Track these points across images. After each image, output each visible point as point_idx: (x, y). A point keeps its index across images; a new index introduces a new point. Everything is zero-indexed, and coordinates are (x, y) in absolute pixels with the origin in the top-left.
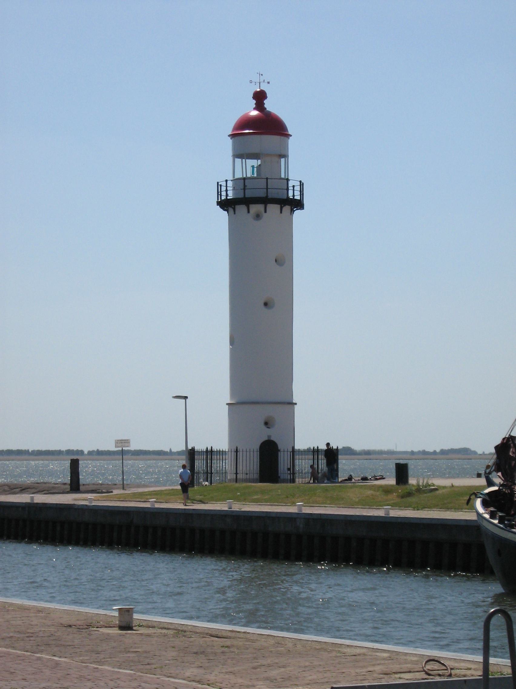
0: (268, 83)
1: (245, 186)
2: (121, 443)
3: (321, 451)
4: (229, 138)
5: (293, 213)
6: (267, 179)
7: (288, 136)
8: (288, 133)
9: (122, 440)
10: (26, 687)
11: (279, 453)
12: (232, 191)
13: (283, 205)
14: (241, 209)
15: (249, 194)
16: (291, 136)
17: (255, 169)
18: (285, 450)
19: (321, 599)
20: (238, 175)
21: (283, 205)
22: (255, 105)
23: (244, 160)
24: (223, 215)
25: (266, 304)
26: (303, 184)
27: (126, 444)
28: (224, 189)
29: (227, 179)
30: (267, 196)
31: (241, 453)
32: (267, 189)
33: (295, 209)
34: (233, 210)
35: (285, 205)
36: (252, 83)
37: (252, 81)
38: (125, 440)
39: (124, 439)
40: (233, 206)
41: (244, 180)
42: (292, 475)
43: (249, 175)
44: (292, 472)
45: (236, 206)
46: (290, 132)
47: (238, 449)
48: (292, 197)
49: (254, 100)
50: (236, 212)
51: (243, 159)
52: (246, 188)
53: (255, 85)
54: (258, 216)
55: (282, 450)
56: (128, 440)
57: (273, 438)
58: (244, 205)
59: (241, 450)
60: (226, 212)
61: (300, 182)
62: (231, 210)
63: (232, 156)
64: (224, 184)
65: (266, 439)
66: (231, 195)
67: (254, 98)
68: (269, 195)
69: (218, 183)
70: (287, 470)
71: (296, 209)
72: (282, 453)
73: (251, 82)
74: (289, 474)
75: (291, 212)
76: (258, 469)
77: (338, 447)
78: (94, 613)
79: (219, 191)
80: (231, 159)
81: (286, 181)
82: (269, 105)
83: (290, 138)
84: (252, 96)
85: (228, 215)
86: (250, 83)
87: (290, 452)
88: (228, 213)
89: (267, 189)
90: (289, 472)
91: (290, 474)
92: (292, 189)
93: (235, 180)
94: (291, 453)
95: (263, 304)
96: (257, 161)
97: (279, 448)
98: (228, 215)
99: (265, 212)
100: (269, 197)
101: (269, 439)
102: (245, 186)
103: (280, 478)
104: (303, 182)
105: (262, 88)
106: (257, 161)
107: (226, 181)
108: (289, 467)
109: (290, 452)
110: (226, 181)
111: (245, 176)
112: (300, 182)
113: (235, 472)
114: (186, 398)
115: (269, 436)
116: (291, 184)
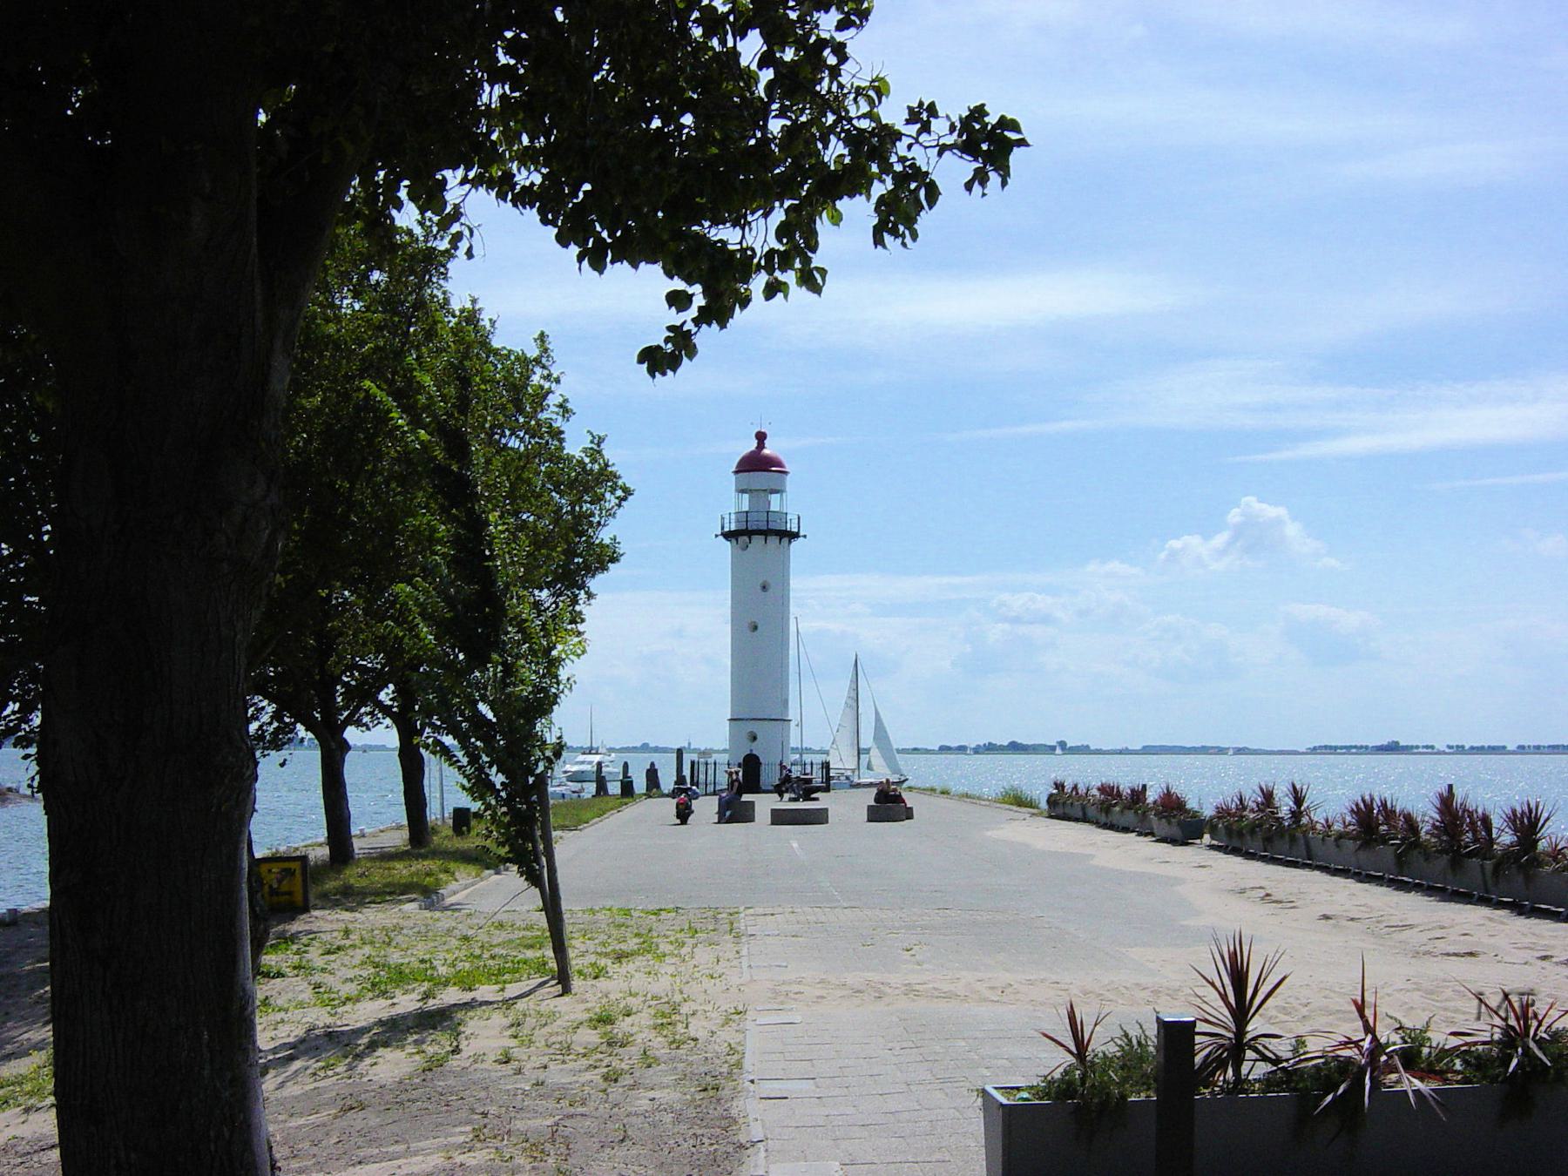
57: (754, 752)
62: (734, 541)
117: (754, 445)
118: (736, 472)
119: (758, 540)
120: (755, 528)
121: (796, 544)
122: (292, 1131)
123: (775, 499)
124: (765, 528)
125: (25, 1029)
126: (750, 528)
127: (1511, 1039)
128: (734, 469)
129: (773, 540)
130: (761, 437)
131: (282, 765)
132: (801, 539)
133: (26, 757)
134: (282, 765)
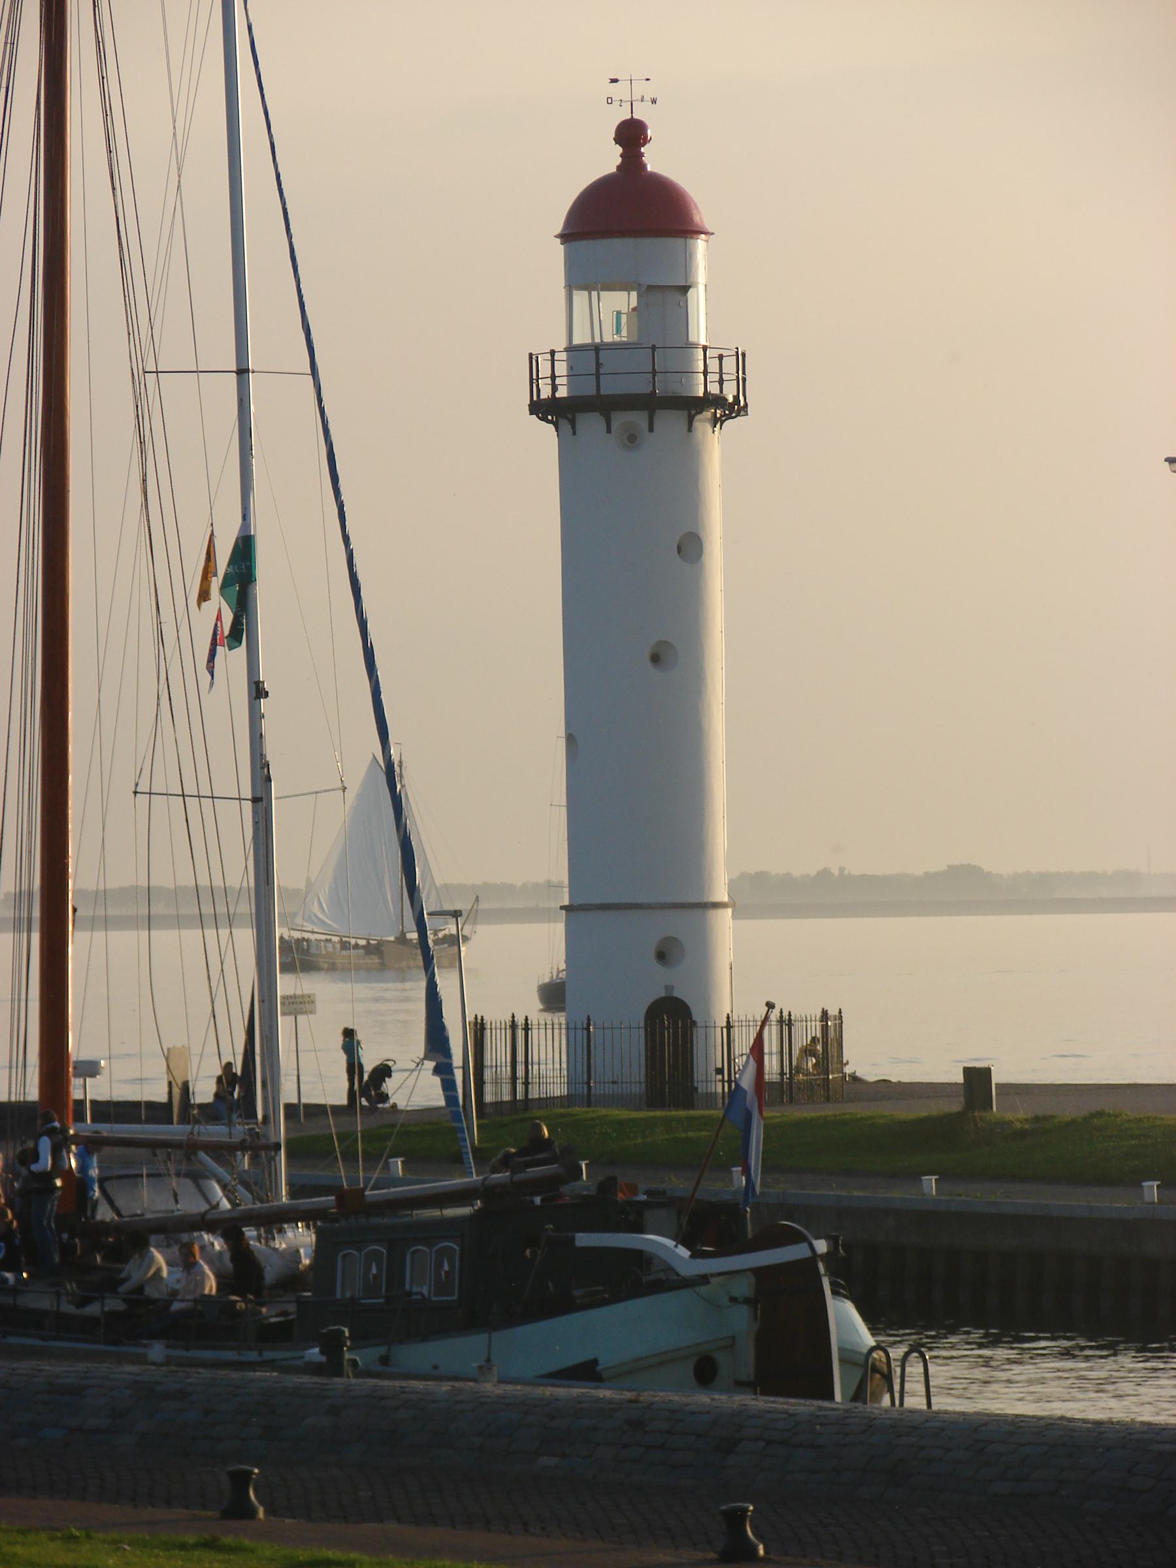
0: (654, 101)
1: (598, 365)
6: (654, 348)
12: (566, 377)
13: (693, 412)
14: (591, 423)
15: (610, 387)
17: (624, 319)
19: (762, 1559)
20: (581, 337)
21: (693, 412)
22: (620, 159)
23: (594, 294)
24: (546, 434)
25: (655, 659)
26: (744, 355)
28: (545, 370)
31: (535, 1032)
34: (570, 426)
36: (611, 103)
37: (611, 98)
40: (570, 416)
41: (596, 353)
42: (726, 1084)
43: (608, 338)
44: (726, 1078)
45: (576, 414)
47: (529, 1022)
49: (617, 145)
50: (577, 424)
51: (594, 290)
52: (601, 372)
53: (620, 106)
54: (632, 439)
57: (677, 994)
58: (597, 414)
59: (535, 1022)
62: (565, 425)
63: (564, 287)
65: (662, 993)
66: (562, 393)
67: (618, 139)
69: (531, 355)
70: (714, 1073)
73: (610, 101)
74: (720, 1081)
76: (643, 1071)
79: (534, 377)
80: (562, 293)
84: (614, 136)
85: (558, 435)
87: (720, 1029)
88: (557, 431)
90: (720, 1077)
91: (723, 1081)
93: (571, 349)
94: (725, 1030)
95: (647, 660)
96: (629, 294)
98: (556, 436)
99: (651, 429)
102: (598, 365)
103: (697, 1092)
106: (629, 294)
107: (553, 353)
108: (720, 1066)
109: (722, 1028)
111: (598, 340)
113: (530, 1086)
115: (669, 988)
132: (654, 160)
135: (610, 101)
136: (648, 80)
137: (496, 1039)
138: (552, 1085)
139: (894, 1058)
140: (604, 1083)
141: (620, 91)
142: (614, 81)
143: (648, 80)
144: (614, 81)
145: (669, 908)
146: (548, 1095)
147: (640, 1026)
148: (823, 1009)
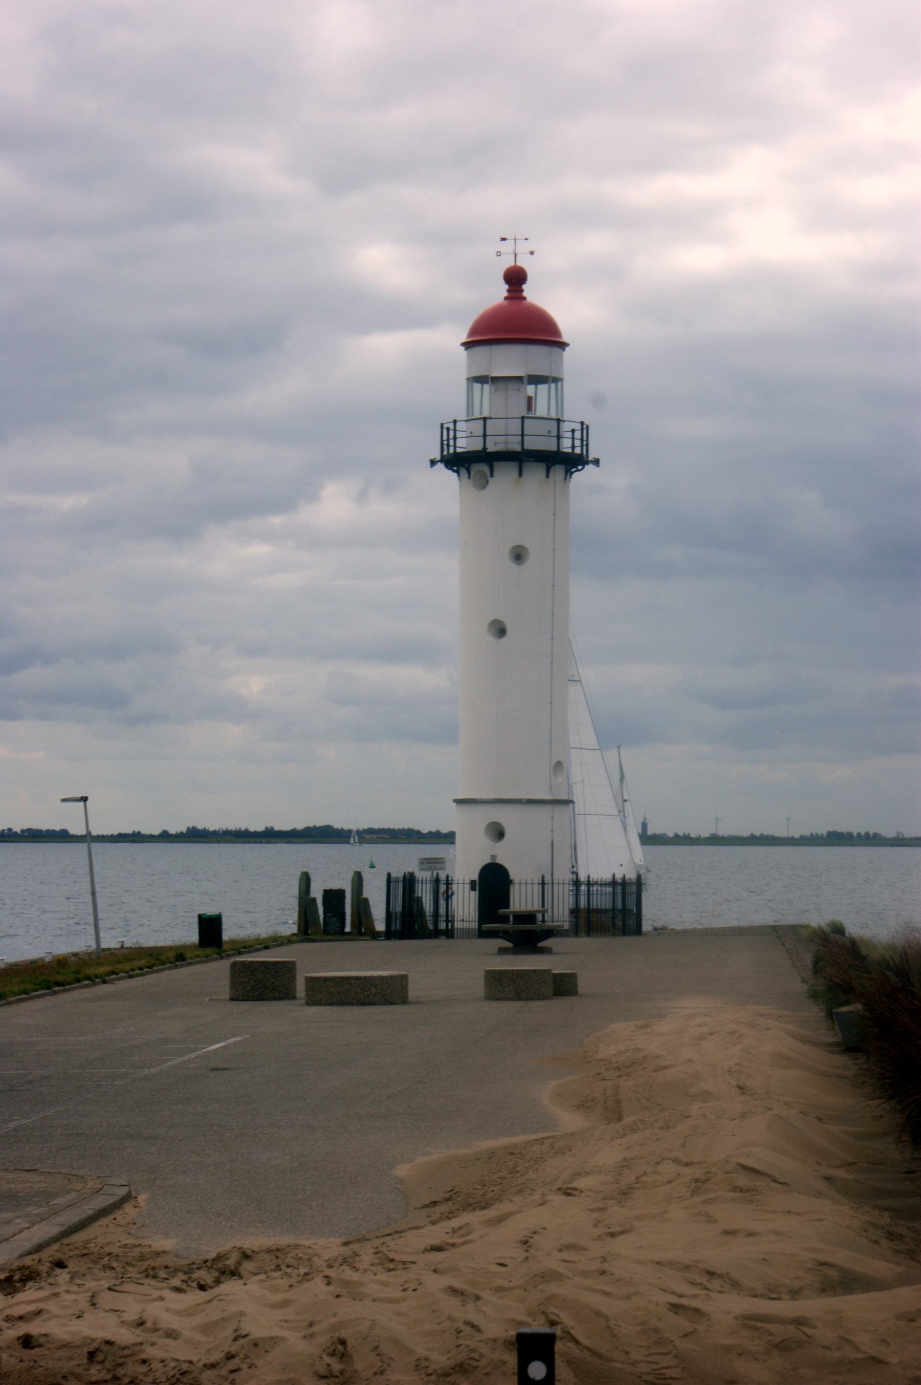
2: (429, 863)
3: (553, 884)
4: (463, 348)
5: (571, 477)
7: (563, 345)
8: (562, 340)
9: (431, 859)
10: (413, 1263)
11: (512, 887)
13: (550, 464)
16: (567, 346)
18: (522, 881)
26: (588, 427)
27: (438, 866)
29: (454, 419)
30: (485, 448)
32: (523, 435)
33: (573, 470)
35: (554, 464)
38: (438, 859)
39: (434, 856)
40: (466, 465)
46: (565, 338)
47: (450, 879)
48: (570, 450)
55: (516, 881)
56: (441, 859)
57: (499, 861)
60: (455, 475)
61: (582, 423)
62: (463, 472)
64: (451, 426)
65: (488, 860)
68: (487, 446)
69: (442, 425)
71: (575, 469)
72: (517, 887)
75: (566, 475)
77: (616, 874)
78: (537, 1140)
81: (555, 423)
82: (532, 293)
83: (567, 349)
86: (498, 256)
89: (523, 435)
92: (571, 436)
97: (511, 878)
100: (488, 451)
101: (493, 862)
104: (588, 424)
105: (519, 264)
110: (455, 422)
112: (582, 423)
114: (84, 799)
115: (493, 857)
116: (566, 427)
117: (499, 292)
118: (468, 345)
119: (505, 476)
120: (500, 448)
121: (583, 477)
122: (27, 1124)
123: (542, 394)
124: (518, 448)
125: (43, 992)
126: (491, 448)
127: (122, 946)
128: (464, 338)
129: (535, 474)
130: (433, 463)
131: (545, 1229)
132: (590, 468)
133: (127, 944)
134: (545, 1229)
135: (499, 254)
136: (526, 239)
137: (422, 891)
138: (599, 896)
139: (139, 1284)
140: (469, 921)
141: (507, 247)
142: (504, 239)
143: (526, 239)
144: (504, 239)
145: (524, 803)
146: (583, 903)
147: (465, 882)
148: (389, 875)
